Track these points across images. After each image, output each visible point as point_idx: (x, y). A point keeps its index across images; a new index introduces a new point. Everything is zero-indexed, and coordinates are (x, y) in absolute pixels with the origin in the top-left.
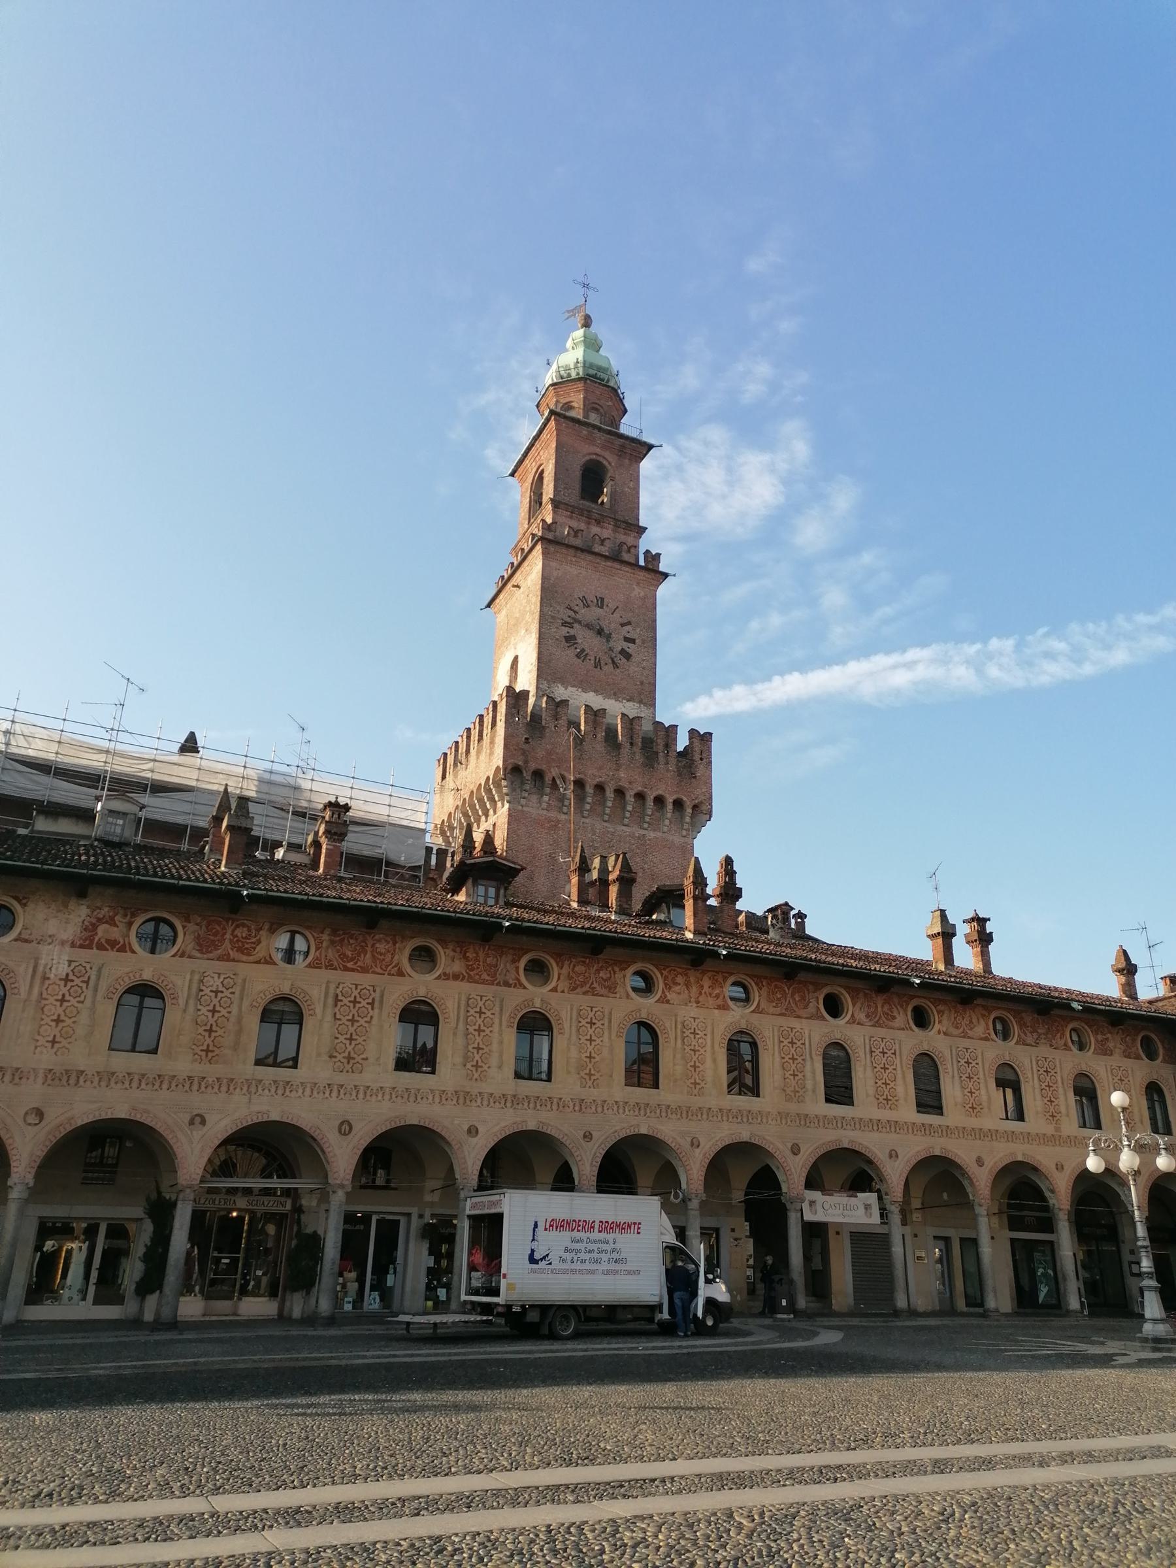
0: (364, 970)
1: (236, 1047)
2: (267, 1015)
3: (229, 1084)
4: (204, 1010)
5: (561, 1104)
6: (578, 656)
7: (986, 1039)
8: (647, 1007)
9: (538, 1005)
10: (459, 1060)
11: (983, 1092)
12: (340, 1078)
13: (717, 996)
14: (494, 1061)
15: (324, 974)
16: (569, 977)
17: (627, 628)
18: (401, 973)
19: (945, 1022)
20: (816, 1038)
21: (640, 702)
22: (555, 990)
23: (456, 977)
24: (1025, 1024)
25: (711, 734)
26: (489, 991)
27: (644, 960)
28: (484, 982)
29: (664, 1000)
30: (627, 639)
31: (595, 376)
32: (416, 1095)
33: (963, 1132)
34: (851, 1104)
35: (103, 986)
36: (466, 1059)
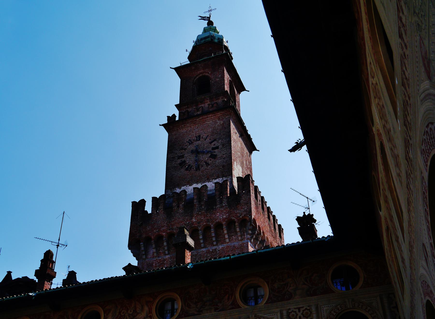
6: (187, 169)
17: (215, 142)
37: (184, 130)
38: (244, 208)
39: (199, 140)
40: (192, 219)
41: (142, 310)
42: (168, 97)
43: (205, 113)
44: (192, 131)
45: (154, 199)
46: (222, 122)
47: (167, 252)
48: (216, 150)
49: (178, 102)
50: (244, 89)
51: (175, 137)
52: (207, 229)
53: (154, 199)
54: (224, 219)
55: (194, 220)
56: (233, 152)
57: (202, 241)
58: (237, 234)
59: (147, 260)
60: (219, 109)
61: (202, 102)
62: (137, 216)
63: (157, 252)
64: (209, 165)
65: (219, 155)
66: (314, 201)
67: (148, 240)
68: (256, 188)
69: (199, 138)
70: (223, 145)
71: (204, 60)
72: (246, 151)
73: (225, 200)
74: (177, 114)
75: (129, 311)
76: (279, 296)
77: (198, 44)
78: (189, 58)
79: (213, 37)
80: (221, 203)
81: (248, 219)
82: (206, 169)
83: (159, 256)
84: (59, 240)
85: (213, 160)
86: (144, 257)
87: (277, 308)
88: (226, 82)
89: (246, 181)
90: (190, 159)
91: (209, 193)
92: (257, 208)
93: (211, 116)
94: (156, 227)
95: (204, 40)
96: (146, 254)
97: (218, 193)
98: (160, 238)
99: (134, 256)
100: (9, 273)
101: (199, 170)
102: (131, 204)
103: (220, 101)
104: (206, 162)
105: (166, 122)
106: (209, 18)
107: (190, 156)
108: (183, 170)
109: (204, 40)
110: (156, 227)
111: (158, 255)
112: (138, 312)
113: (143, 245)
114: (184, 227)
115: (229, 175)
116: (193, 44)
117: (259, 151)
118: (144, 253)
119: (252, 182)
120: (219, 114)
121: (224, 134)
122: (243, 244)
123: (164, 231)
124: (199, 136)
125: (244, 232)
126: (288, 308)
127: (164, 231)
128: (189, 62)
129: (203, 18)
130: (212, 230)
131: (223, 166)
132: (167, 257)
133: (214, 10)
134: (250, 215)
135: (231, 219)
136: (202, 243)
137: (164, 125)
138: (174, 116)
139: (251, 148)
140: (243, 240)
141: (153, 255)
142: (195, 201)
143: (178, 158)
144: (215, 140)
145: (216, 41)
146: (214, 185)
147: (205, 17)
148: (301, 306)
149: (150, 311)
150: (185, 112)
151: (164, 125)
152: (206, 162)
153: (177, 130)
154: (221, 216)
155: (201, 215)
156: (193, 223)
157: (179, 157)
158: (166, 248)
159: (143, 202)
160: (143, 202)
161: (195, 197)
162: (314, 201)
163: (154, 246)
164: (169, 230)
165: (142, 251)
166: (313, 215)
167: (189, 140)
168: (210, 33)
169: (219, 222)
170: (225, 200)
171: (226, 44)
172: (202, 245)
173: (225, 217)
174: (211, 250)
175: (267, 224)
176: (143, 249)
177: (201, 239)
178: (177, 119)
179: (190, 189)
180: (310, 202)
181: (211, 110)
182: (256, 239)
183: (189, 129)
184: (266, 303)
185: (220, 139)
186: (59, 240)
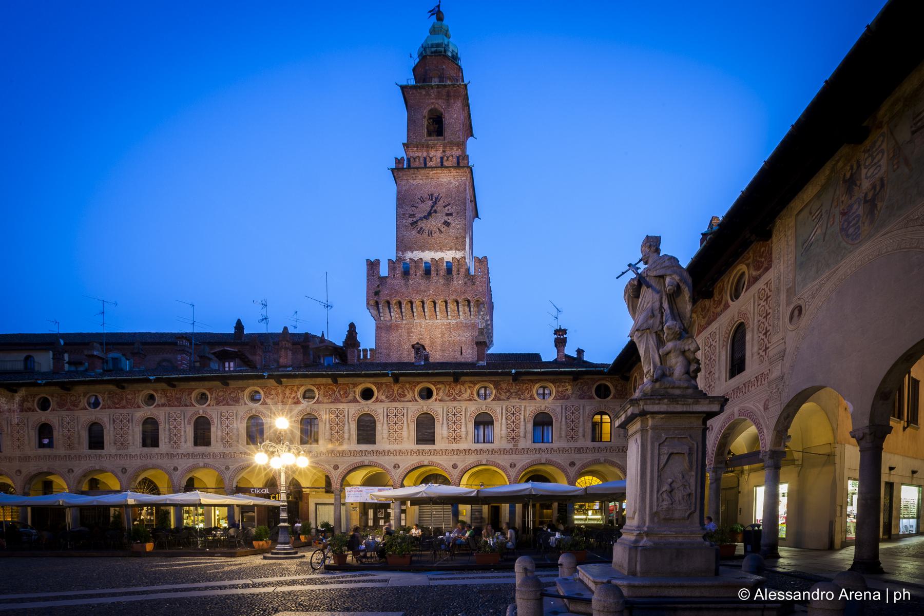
0: (124, 407)
1: (79, 443)
2: (477, 424)
3: (79, 457)
4: (65, 430)
5: (215, 455)
6: (419, 232)
7: (470, 400)
8: (424, 406)
9: (201, 413)
10: (167, 440)
11: (463, 429)
12: (120, 452)
13: (294, 398)
14: (183, 440)
15: (108, 411)
16: (216, 398)
17: (449, 207)
18: (139, 407)
19: (441, 394)
20: (352, 412)
21: (456, 249)
22: (209, 405)
23: (163, 405)
24: (501, 389)
25: (486, 258)
26: (178, 410)
27: (254, 385)
28: (176, 406)
29: (265, 403)
30: (447, 215)
31: (436, 52)
32: (151, 456)
33: (446, 452)
34: (374, 443)
35: (30, 425)
36: (170, 440)
37: (415, 183)
50: (472, 135)
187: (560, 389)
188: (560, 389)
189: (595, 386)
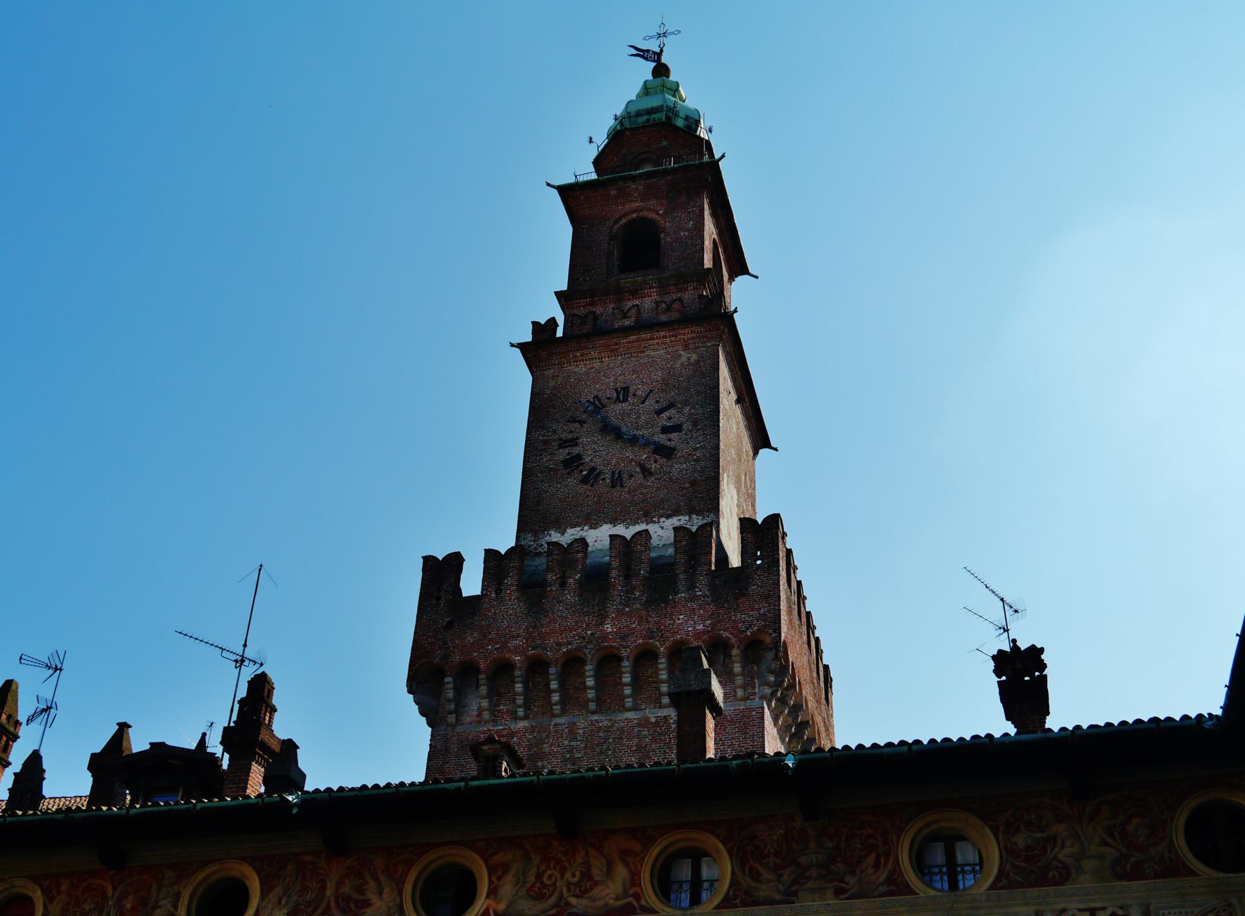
6: (584, 480)
17: (672, 412)
19: (507, 890)
37: (581, 369)
38: (759, 609)
39: (625, 400)
40: (602, 624)
41: (609, 873)
42: (537, 268)
43: (642, 326)
44: (599, 372)
45: (490, 555)
46: (694, 357)
47: (521, 712)
48: (674, 435)
49: (564, 286)
50: (745, 271)
51: (552, 383)
52: (646, 656)
53: (490, 555)
54: (698, 635)
55: (608, 628)
56: (722, 446)
57: (628, 691)
58: (733, 682)
59: (459, 729)
60: (686, 320)
61: (635, 292)
62: (438, 598)
63: (493, 710)
64: (651, 474)
65: (683, 450)
66: (1016, 611)
67: (468, 672)
68: (789, 553)
69: (623, 394)
70: (695, 423)
71: (648, 175)
72: (747, 446)
73: (702, 581)
74: (560, 319)
75: (568, 875)
76: (1029, 871)
77: (628, 125)
78: (597, 163)
79: (672, 111)
80: (692, 587)
81: (768, 640)
82: (641, 485)
83: (495, 722)
84: (245, 645)
85: (663, 461)
86: (452, 719)
87: (1027, 904)
88: (708, 244)
89: (764, 535)
90: (598, 452)
91: (653, 555)
92: (790, 612)
93: (665, 337)
94: (492, 635)
95: (645, 117)
96: (458, 712)
97: (682, 559)
98: (502, 669)
99: (422, 713)
100: (123, 727)
101: (622, 486)
102: (420, 564)
103: (689, 295)
104: (643, 467)
105: (528, 338)
106: (659, 55)
107: (595, 442)
108: (572, 481)
109: (645, 117)
110: (492, 635)
111: (496, 716)
112: (597, 878)
113: (451, 686)
114: (700, 647)
115: (709, 511)
116: (610, 123)
117: (776, 449)
118: (452, 706)
119: (783, 538)
120: (687, 333)
121: (698, 393)
122: (750, 710)
123: (516, 651)
124: (626, 390)
125: (752, 678)
126: (1060, 906)
127: (516, 651)
128: (594, 176)
129: (643, 54)
130: (663, 662)
131: (693, 483)
132: (522, 724)
133: (673, 33)
134: (774, 631)
135: (721, 637)
136: (628, 697)
137: (522, 347)
138: (552, 322)
139: (760, 439)
140: (748, 698)
141: (479, 715)
142: (614, 573)
143: (560, 446)
144: (672, 405)
145: (680, 123)
146: (671, 534)
147: (648, 51)
148: (1098, 905)
149: (635, 880)
150: (586, 315)
151: (522, 347)
152: (643, 467)
153: (561, 364)
154: (689, 622)
155: (629, 615)
156: (604, 636)
157: (564, 444)
158: (520, 701)
159: (456, 561)
160: (456, 561)
161: (615, 564)
162: (1016, 611)
163: (484, 690)
164: (533, 648)
165: (449, 701)
166: (1042, 650)
167: (596, 397)
168: (665, 100)
169: (682, 642)
170: (702, 581)
171: (703, 134)
172: (629, 702)
173: (701, 627)
174: (653, 720)
175: (805, 658)
176: (451, 695)
177: (627, 685)
178: (560, 333)
179: (599, 537)
180: (1009, 612)
181: (664, 318)
182: (783, 701)
183: (597, 364)
184: (993, 887)
185: (686, 403)
186: (245, 645)
187: (1021, 840)
188: (1021, 840)
189: (1193, 802)
